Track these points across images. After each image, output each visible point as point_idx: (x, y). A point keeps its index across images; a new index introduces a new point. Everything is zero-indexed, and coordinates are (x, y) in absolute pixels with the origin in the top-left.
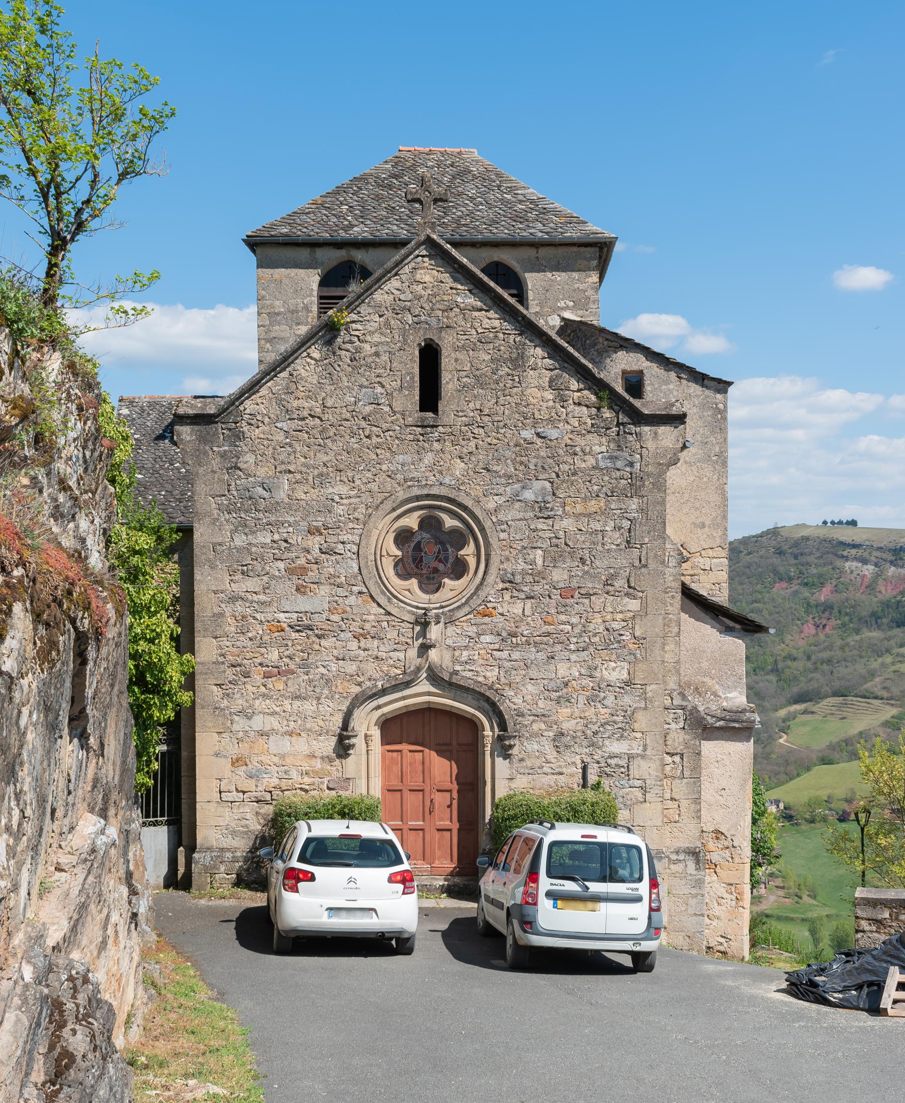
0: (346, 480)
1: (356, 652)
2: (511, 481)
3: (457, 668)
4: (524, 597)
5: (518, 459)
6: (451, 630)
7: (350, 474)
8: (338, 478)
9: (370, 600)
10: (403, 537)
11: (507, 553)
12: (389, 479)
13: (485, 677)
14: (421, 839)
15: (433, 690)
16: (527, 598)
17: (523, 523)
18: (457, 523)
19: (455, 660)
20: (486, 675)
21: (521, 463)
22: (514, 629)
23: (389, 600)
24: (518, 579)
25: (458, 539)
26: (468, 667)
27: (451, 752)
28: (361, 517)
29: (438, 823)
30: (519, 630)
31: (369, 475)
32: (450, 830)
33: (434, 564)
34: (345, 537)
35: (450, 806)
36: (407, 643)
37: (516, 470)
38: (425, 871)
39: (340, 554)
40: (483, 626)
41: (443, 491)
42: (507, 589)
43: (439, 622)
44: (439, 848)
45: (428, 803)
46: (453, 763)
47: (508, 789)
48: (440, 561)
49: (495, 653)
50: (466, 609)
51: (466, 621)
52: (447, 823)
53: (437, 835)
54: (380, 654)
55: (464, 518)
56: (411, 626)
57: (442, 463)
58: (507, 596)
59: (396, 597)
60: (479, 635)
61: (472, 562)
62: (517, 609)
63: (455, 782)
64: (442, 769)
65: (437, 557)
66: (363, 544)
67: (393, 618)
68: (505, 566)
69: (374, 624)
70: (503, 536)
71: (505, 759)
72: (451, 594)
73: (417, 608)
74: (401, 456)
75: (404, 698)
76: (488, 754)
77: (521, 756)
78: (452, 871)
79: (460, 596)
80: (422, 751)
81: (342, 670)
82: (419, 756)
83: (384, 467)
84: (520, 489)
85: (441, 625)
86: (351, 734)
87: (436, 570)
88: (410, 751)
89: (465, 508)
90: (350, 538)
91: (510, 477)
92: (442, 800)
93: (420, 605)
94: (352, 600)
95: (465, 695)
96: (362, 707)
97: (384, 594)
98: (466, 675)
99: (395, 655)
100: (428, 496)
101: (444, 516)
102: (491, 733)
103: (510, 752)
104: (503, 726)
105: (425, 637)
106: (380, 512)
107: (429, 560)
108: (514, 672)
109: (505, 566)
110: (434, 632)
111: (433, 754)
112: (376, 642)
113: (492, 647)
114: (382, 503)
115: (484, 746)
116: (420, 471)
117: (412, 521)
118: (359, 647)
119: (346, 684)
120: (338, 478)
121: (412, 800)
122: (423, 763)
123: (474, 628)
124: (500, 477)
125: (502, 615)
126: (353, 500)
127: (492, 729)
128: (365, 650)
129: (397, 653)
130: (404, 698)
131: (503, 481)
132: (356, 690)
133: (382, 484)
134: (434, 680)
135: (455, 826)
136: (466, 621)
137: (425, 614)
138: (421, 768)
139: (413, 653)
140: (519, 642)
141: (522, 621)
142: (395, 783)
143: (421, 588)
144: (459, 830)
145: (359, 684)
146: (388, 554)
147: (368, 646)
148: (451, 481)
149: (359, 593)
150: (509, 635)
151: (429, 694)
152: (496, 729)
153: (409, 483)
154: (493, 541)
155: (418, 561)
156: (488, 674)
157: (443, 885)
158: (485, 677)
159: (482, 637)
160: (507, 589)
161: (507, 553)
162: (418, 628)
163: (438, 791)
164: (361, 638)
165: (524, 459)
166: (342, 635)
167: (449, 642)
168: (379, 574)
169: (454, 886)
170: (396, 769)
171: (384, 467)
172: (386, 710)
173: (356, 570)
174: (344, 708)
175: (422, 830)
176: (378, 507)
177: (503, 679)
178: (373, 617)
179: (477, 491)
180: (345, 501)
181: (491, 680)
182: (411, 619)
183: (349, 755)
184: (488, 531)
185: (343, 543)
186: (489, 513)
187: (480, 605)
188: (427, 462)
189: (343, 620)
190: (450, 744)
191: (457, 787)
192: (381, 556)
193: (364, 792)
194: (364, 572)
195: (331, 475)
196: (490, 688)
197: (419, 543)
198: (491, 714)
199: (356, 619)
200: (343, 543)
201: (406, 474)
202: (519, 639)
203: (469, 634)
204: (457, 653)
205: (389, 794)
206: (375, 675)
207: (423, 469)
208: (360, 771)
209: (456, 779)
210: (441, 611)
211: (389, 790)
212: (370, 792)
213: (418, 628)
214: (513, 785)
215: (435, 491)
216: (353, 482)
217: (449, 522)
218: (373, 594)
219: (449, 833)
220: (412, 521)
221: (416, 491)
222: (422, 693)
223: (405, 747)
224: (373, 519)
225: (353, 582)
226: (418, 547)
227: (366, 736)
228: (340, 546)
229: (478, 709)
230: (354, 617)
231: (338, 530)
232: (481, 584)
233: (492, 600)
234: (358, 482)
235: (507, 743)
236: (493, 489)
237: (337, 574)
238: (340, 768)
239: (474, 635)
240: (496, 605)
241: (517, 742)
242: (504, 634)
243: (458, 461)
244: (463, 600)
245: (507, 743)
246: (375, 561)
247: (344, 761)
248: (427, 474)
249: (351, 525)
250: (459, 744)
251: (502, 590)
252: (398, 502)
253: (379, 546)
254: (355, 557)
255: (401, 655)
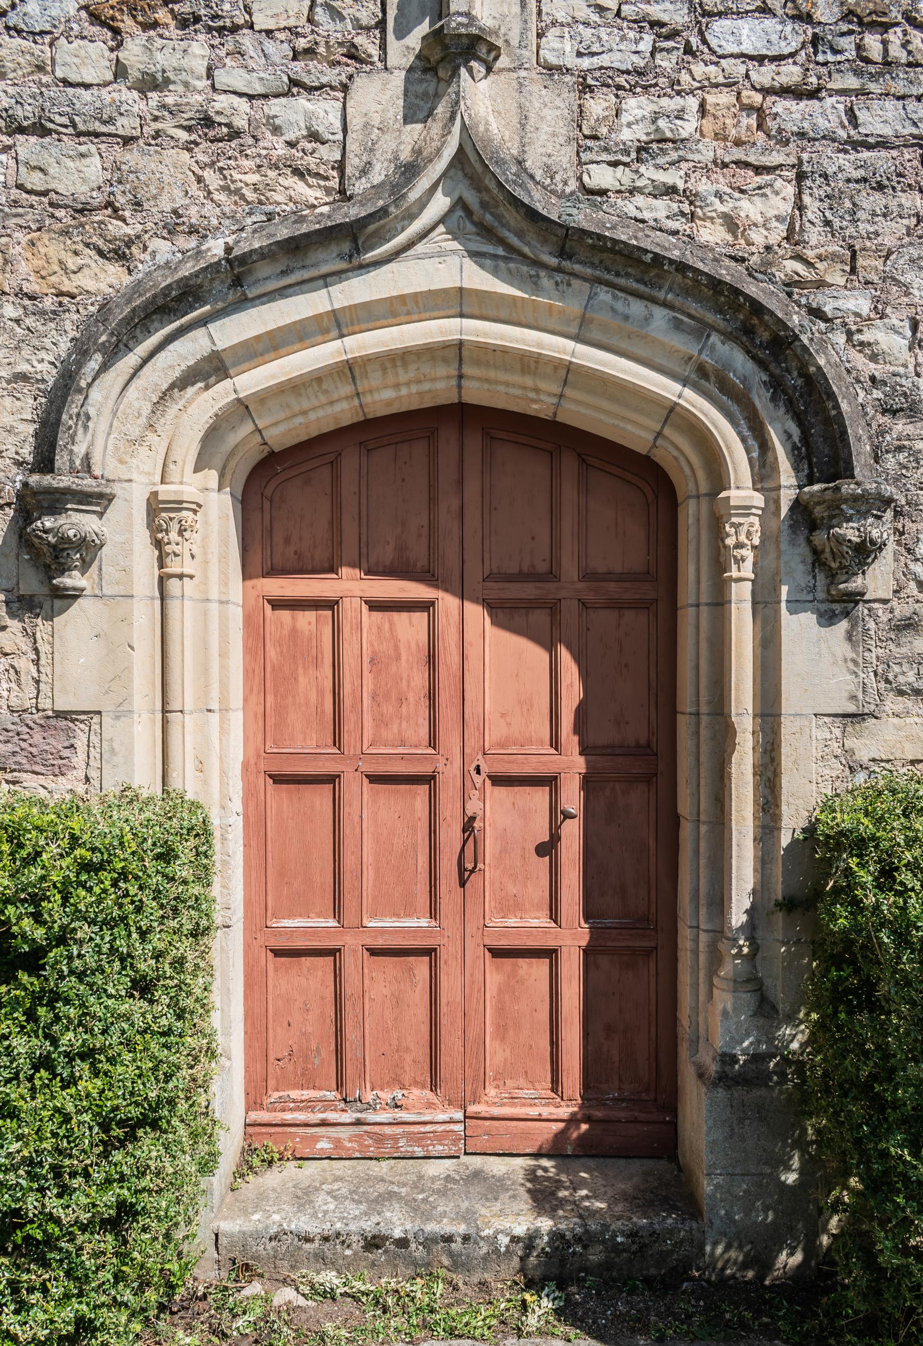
3: (601, 176)
13: (731, 223)
14: (419, 997)
15: (479, 279)
19: (587, 140)
20: (741, 222)
26: (649, 173)
27: (553, 608)
29: (495, 921)
32: (550, 954)
35: (548, 848)
38: (440, 1137)
44: (502, 1032)
45: (450, 836)
46: (565, 655)
47: (836, 768)
49: (781, 106)
52: (532, 924)
53: (495, 975)
54: (223, 102)
63: (570, 740)
64: (517, 685)
71: (828, 619)
75: (339, 323)
76: (741, 596)
77: (901, 610)
78: (560, 1137)
80: (426, 606)
81: (35, 180)
82: (410, 629)
86: (64, 481)
88: (376, 606)
92: (511, 821)
95: (637, 308)
96: (131, 360)
98: (641, 215)
99: (295, 112)
102: (758, 500)
103: (857, 583)
104: (824, 450)
108: (871, 201)
111: (475, 612)
112: (199, 50)
113: (764, 75)
115: (720, 561)
118: (120, 71)
119: (52, 248)
121: (384, 823)
122: (432, 660)
127: (764, 473)
129: (302, 103)
130: (339, 323)
132: (104, 279)
134: (486, 232)
135: (573, 937)
138: (420, 679)
139: (379, 96)
140: (896, 52)
142: (307, 743)
144: (587, 952)
145: (119, 253)
151: (460, 302)
152: (787, 477)
156: (749, 209)
157: (529, 1241)
158: (731, 223)
159: (719, 26)
163: (499, 780)
167: (559, 48)
169: (586, 1239)
170: (312, 685)
172: (251, 381)
174: (45, 369)
175: (429, 952)
177: (814, 235)
181: (758, 237)
183: (69, 597)
190: (552, 575)
191: (579, 764)
193: (146, 780)
196: (762, 272)
198: (761, 400)
202: (895, 37)
204: (598, 106)
205: (280, 800)
206: (197, 204)
208: (119, 677)
209: (579, 727)
211: (279, 779)
212: (175, 783)
214: (866, 746)
219: (541, 967)
222: (427, 307)
223: (350, 585)
227: (156, 508)
229: (702, 377)
235: (850, 532)
238: (24, 664)
241: (880, 529)
245: (850, 532)
247: (42, 628)
250: (588, 576)
255: (324, 112)
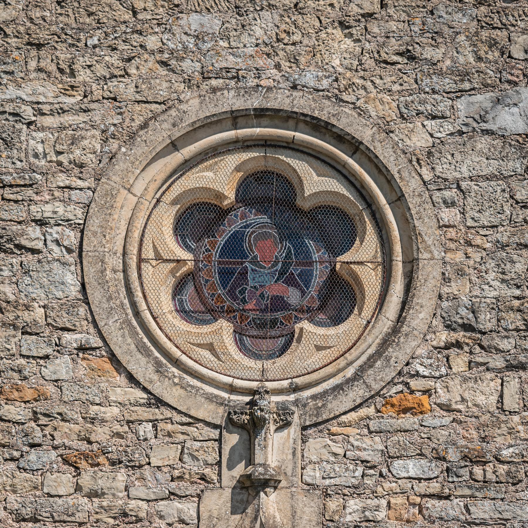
0: (52, 68)
1: (70, 501)
2: (467, 86)
4: (498, 362)
5: (485, 34)
6: (317, 446)
7: (64, 54)
8: (33, 64)
9: (108, 366)
10: (198, 219)
11: (459, 257)
12: (162, 71)
16: (510, 367)
17: (498, 186)
18: (335, 185)
21: (492, 44)
22: (477, 445)
23: (159, 368)
24: (486, 320)
25: (335, 227)
28: (89, 159)
30: (491, 447)
31: (114, 59)
33: (276, 289)
34: (48, 208)
36: (203, 478)
37: (479, 59)
39: (34, 251)
40: (400, 437)
41: (301, 103)
42: (458, 345)
43: (287, 424)
48: (291, 281)
49: (430, 503)
50: (358, 393)
51: (357, 424)
54: (133, 504)
55: (354, 174)
56: (215, 434)
57: (297, 37)
58: (459, 363)
59: (176, 363)
60: (389, 458)
61: (370, 279)
62: (485, 393)
65: (282, 273)
66: (94, 224)
67: (168, 413)
68: (454, 288)
69: (117, 428)
70: (448, 215)
72: (317, 359)
73: (232, 389)
74: (194, 17)
79: (342, 362)
83: (152, 42)
84: (488, 105)
85: (294, 431)
87: (279, 304)
89: (354, 147)
90: (61, 210)
91: (464, 75)
93: (239, 383)
94: (61, 367)
97: (147, 354)
100: (261, 115)
101: (301, 167)
105: (250, 462)
106: (141, 150)
107: (264, 281)
109: (454, 288)
110: (275, 449)
112: (121, 476)
113: (422, 487)
114: (144, 126)
116: (243, 50)
117: (222, 178)
118: (78, 488)
120: (33, 64)
123: (378, 442)
124: (441, 74)
125: (447, 408)
126: (68, 119)
128: (93, 494)
129: (176, 504)
131: (448, 83)
133: (146, 80)
136: (357, 424)
137: (252, 403)
140: (490, 476)
141: (498, 423)
143: (242, 347)
146: (158, 257)
147: (102, 483)
148: (319, 79)
149: (82, 349)
150: (465, 457)
153: (214, 82)
154: (427, 228)
155: (232, 277)
159: (397, 464)
160: (458, 345)
161: (459, 257)
162: (232, 439)
164: (83, 464)
165: (501, 35)
166: (33, 456)
167: (313, 474)
168: (134, 305)
171: (152, 42)
173: (74, 291)
176: (132, 136)
178: (116, 410)
179: (384, 107)
180: (48, 121)
182: (218, 415)
184: (412, 202)
185: (41, 223)
186: (414, 160)
187: (392, 383)
188: (259, 32)
189: (36, 420)
192: (140, 260)
194: (95, 295)
195: (15, 54)
197: (237, 238)
199: (70, 415)
200: (41, 223)
201: (207, 61)
202: (489, 468)
203: (364, 455)
204: (333, 504)
207: (250, 50)
210: (292, 397)
213: (232, 439)
215: (281, 100)
216: (73, 74)
217: (315, 183)
218: (118, 352)
220: (222, 178)
221: (232, 101)
224: (120, 166)
225: (64, 321)
226: (235, 247)
228: (34, 231)
230: (63, 409)
231: (29, 192)
232: (395, 331)
233: (421, 370)
234: (83, 76)
236: (422, 102)
237: (23, 300)
239: (376, 459)
240: (431, 383)
242: (453, 455)
243: (338, 33)
244: (350, 372)
246: (125, 271)
248: (261, 62)
249: (62, 180)
251: (447, 347)
252: (184, 127)
253: (136, 235)
254: (70, 259)
255: (188, 509)
